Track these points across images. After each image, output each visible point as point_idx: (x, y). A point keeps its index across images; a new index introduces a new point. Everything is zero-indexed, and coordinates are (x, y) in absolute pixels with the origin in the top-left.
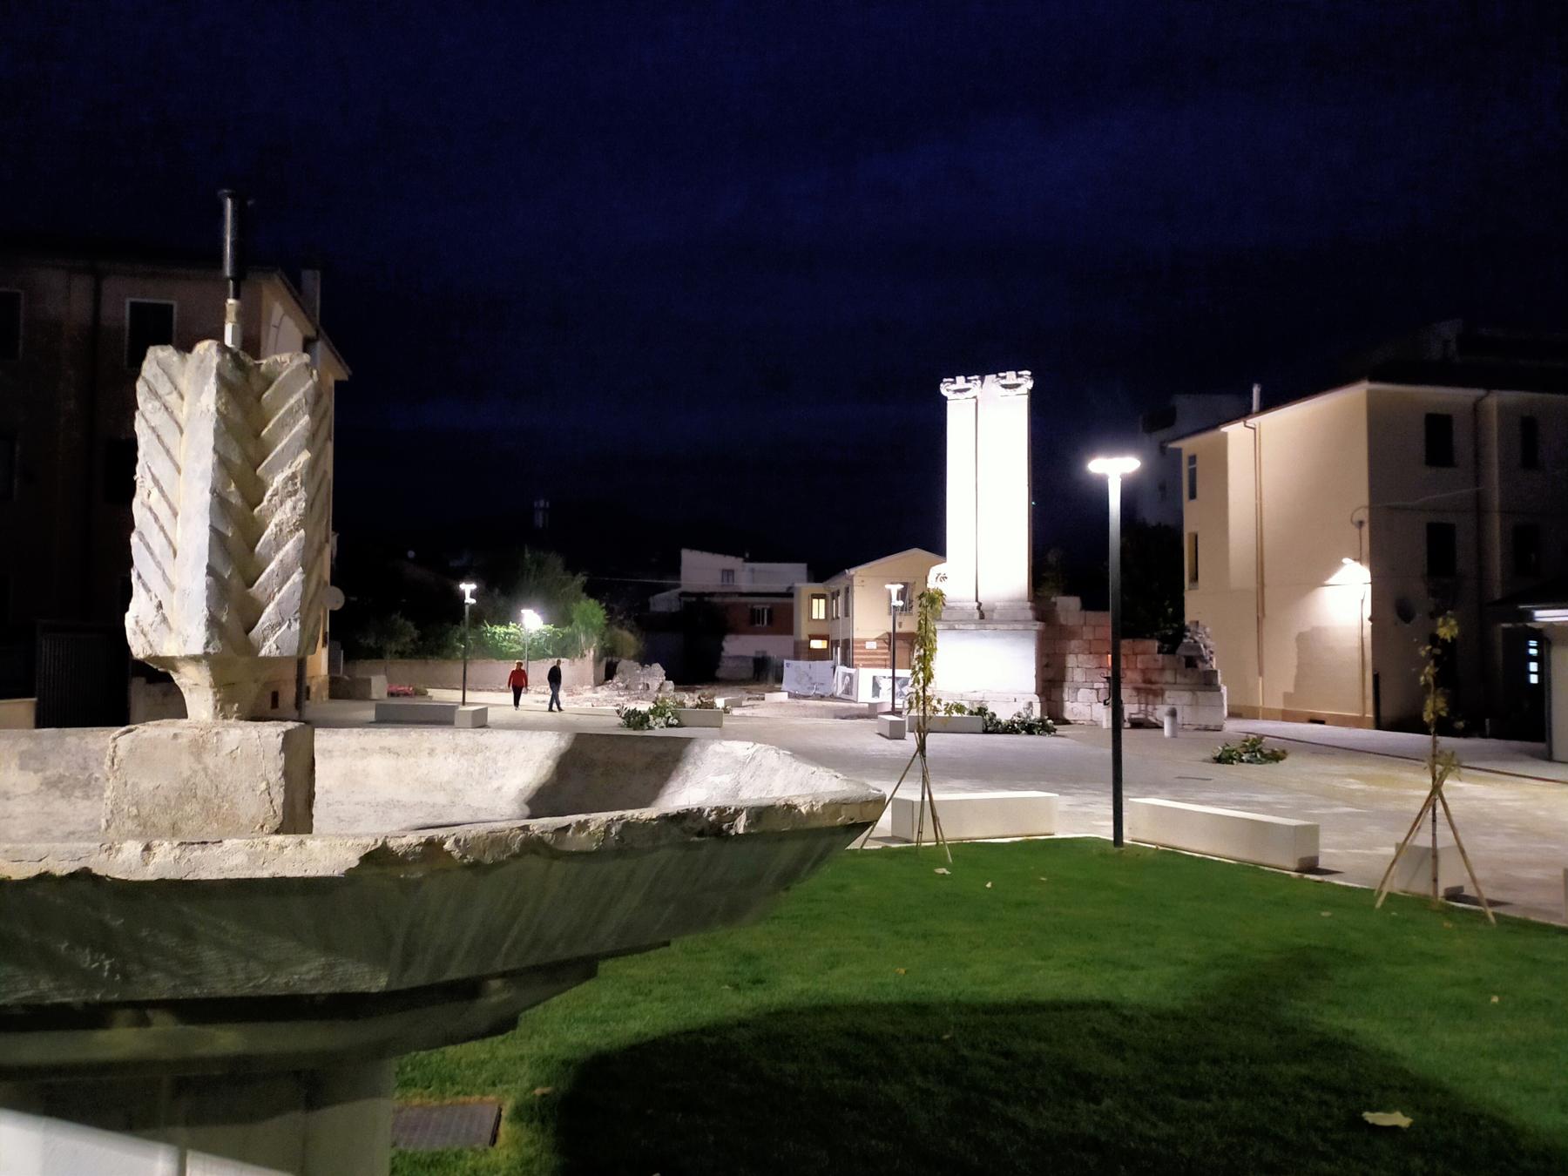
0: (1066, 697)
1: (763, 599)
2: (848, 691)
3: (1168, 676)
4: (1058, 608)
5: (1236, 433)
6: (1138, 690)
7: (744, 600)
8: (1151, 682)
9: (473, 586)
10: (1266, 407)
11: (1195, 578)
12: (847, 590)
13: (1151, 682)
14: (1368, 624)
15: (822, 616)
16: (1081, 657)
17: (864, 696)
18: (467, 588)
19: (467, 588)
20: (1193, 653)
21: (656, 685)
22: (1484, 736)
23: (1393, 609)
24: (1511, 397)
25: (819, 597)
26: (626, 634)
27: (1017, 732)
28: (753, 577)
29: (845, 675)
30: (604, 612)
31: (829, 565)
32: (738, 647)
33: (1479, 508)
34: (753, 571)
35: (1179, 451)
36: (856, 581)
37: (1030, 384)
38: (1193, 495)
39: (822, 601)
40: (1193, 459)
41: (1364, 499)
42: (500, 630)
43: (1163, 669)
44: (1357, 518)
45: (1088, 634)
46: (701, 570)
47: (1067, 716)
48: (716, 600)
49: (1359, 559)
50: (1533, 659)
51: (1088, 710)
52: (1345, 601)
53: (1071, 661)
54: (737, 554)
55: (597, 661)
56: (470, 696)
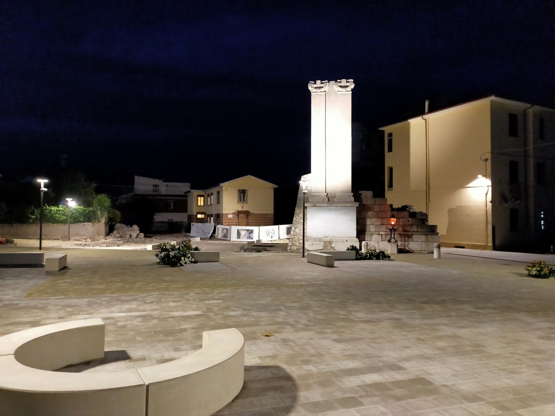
1: (173, 198)
2: (225, 236)
4: (362, 196)
5: (416, 124)
6: (400, 235)
7: (163, 198)
8: (406, 231)
9: (46, 181)
10: (432, 110)
11: (391, 185)
12: (218, 192)
13: (406, 231)
14: (490, 205)
15: (202, 204)
16: (373, 220)
17: (234, 237)
18: (42, 182)
19: (42, 182)
20: (424, 217)
21: (135, 235)
22: (551, 253)
23: (499, 196)
24: (537, 108)
25: (201, 196)
26: (117, 211)
27: (370, 258)
28: (166, 188)
29: (223, 229)
30: (109, 200)
31: (209, 181)
32: (161, 217)
33: (526, 156)
34: (167, 186)
35: (383, 131)
36: (224, 188)
37: (353, 86)
38: (390, 150)
39: (202, 198)
40: (390, 135)
41: (488, 148)
42: (54, 208)
43: (412, 225)
44: (484, 157)
45: (376, 208)
46: (143, 185)
49: (485, 176)
50: (542, 219)
52: (479, 193)
55: (106, 224)
56: (45, 243)
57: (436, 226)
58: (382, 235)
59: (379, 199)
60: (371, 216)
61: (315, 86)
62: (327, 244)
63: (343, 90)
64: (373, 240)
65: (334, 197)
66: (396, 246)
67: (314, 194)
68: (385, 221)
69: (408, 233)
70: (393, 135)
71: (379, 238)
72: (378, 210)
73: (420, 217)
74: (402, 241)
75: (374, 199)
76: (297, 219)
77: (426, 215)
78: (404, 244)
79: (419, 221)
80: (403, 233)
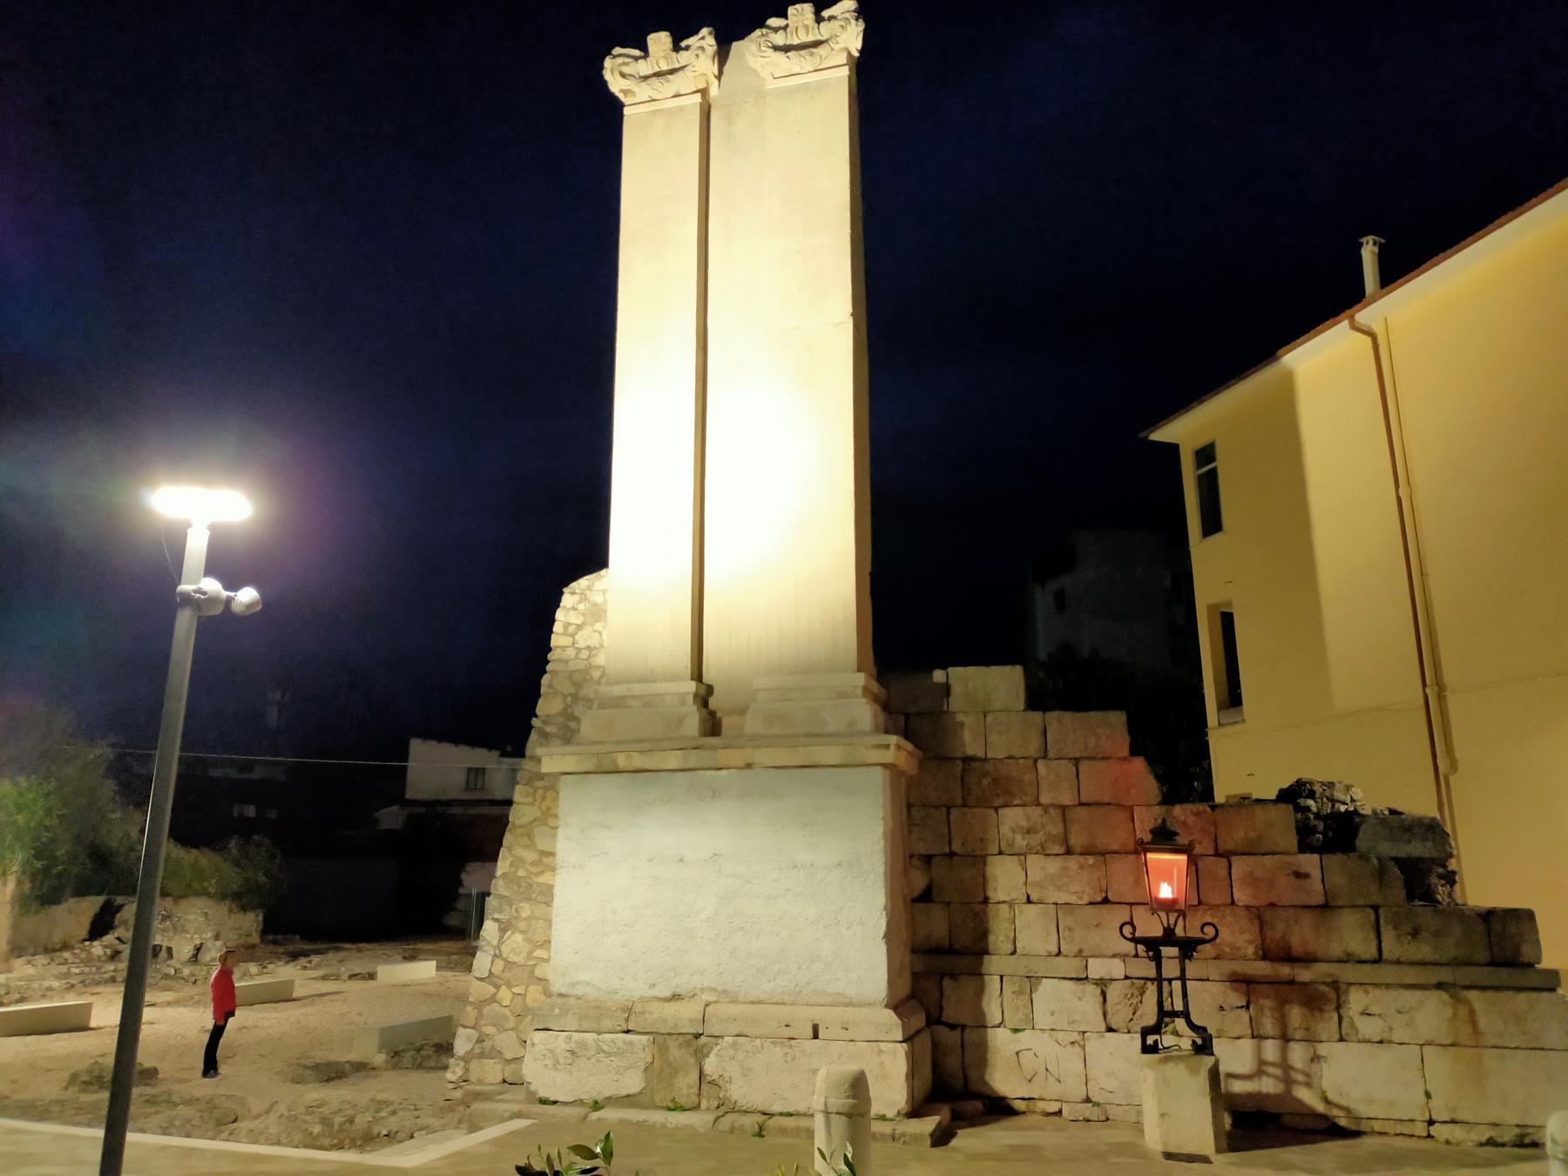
0: (993, 1012)
3: (1351, 934)
4: (956, 702)
6: (1245, 983)
8: (1290, 958)
10: (1392, 274)
11: (1233, 698)
20: (1417, 849)
35: (1172, 450)
38: (1212, 525)
40: (1206, 455)
43: (1326, 907)
45: (1056, 784)
47: (1003, 1082)
48: (457, 810)
51: (1070, 1063)
53: (1005, 878)
54: (489, 746)
57: (1529, 915)
58: (1103, 984)
59: (1068, 717)
60: (1021, 842)
61: (644, 67)
62: (676, 1053)
63: (795, 62)
64: (1042, 1018)
65: (742, 711)
66: (1202, 1082)
67: (616, 691)
68: (1121, 873)
69: (1304, 975)
70: (1220, 452)
71: (1087, 1004)
72: (1067, 798)
73: (1386, 848)
74: (1257, 1036)
75: (1037, 716)
76: (518, 862)
77: (1433, 830)
78: (1285, 1065)
79: (1381, 874)
80: (1262, 968)
